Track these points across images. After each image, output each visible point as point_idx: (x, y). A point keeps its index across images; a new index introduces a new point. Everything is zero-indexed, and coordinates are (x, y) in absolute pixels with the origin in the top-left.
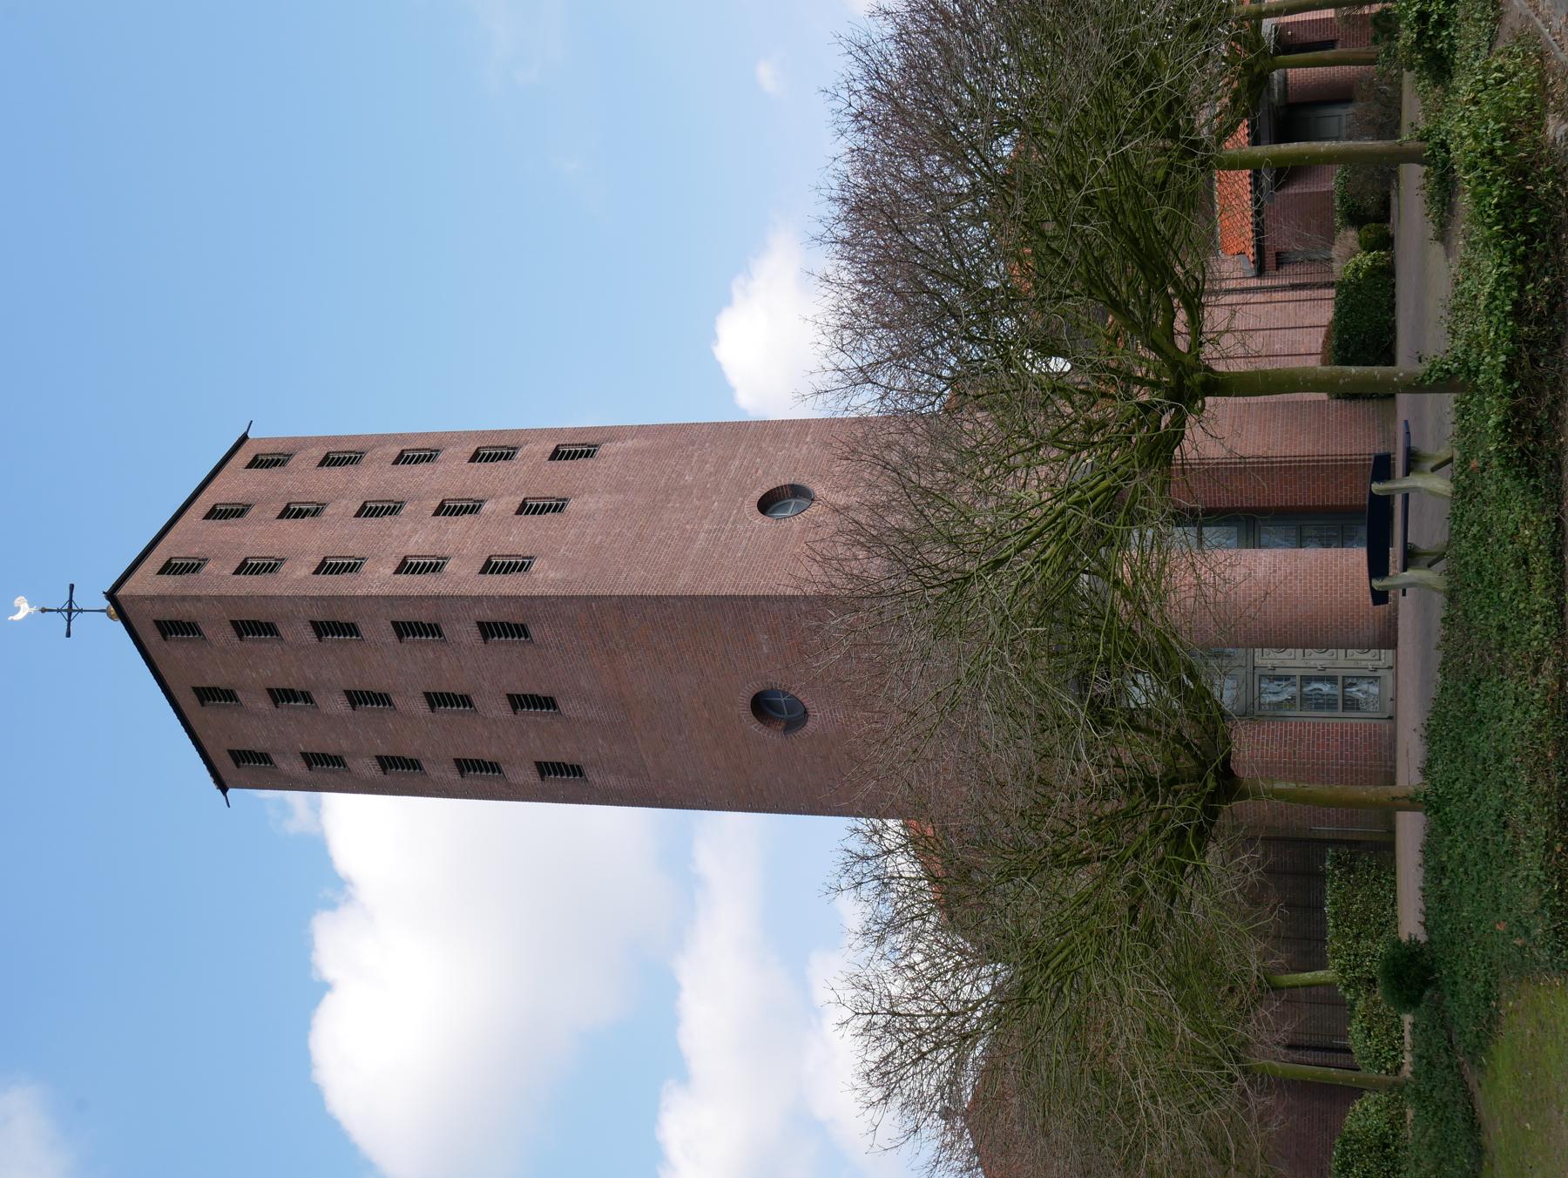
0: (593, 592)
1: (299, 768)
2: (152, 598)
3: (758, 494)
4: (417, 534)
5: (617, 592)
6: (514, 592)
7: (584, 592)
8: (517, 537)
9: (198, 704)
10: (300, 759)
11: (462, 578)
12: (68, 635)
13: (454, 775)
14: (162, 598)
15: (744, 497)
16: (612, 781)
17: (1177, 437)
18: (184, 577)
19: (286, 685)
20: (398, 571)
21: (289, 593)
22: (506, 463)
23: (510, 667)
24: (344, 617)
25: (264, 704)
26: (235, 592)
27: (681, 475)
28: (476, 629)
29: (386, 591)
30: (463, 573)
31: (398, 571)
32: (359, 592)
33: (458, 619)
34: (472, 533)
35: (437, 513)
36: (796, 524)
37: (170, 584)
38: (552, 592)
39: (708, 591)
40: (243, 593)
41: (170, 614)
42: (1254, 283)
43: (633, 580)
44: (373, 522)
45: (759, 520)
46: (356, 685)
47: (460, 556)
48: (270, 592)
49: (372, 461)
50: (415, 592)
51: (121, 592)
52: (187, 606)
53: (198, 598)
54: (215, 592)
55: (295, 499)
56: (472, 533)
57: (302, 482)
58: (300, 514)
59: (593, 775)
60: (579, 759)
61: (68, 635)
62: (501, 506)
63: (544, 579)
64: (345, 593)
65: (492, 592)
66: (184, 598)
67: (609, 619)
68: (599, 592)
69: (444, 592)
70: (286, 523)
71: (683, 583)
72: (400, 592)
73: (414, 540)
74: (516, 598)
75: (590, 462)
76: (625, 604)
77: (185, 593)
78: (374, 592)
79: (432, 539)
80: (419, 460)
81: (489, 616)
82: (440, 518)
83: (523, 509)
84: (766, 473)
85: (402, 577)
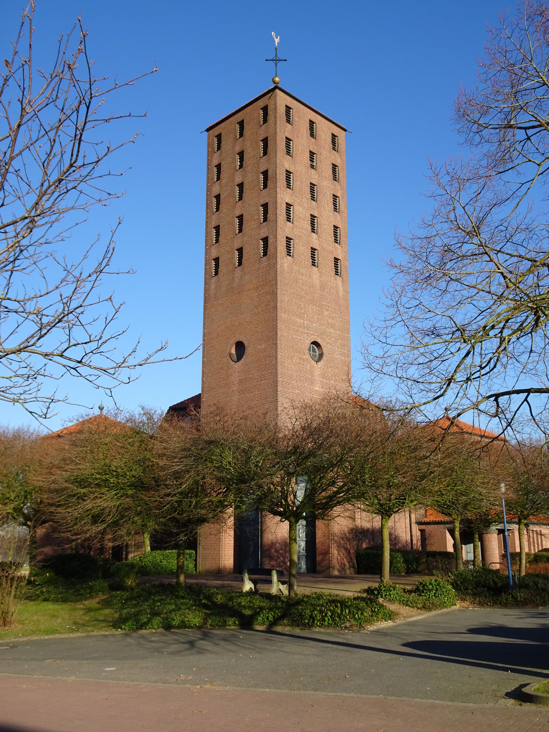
0: (279, 282)
1: (215, 162)
2: (276, 104)
3: (319, 341)
4: (302, 210)
5: (278, 291)
6: (278, 251)
7: (279, 278)
8: (301, 249)
9: (238, 120)
10: (219, 163)
11: (284, 229)
12: (266, 60)
13: (214, 224)
14: (276, 109)
15: (318, 336)
16: (213, 287)
17: (276, 513)
18: (285, 117)
19: (245, 158)
20: (287, 204)
21: (278, 161)
22: (333, 240)
23: (253, 249)
24: (269, 183)
25: (238, 149)
26: (278, 139)
27: (327, 310)
28: (265, 236)
29: (279, 200)
30: (287, 230)
31: (287, 204)
32: (278, 189)
33: (268, 229)
34: (303, 231)
35: (311, 215)
36: (307, 356)
37: (282, 110)
38: (279, 266)
39: (279, 326)
40: (278, 142)
41: (270, 112)
42: (413, 520)
43: (284, 297)
44: (308, 189)
45: (308, 342)
46: (245, 187)
47: (293, 228)
48: (278, 153)
49: (335, 185)
50: (278, 212)
51: (278, 91)
52: (273, 119)
53: (276, 124)
54: (278, 130)
55: (318, 156)
56: (303, 231)
57: (326, 158)
58: (312, 160)
59: (214, 279)
60: (220, 274)
61: (266, 60)
62: (314, 240)
63: (284, 263)
64: (278, 184)
65: (278, 242)
66: (276, 117)
67: (269, 286)
68: (279, 284)
69: (278, 223)
70: (308, 155)
71: (282, 315)
72: (278, 206)
73: (301, 208)
74: (276, 252)
75: (333, 273)
76: (274, 294)
77: (278, 118)
78: (278, 195)
79: (301, 215)
80: (335, 205)
81: (270, 241)
82: (310, 217)
83: (313, 250)
84: (328, 343)
85: (284, 206)
